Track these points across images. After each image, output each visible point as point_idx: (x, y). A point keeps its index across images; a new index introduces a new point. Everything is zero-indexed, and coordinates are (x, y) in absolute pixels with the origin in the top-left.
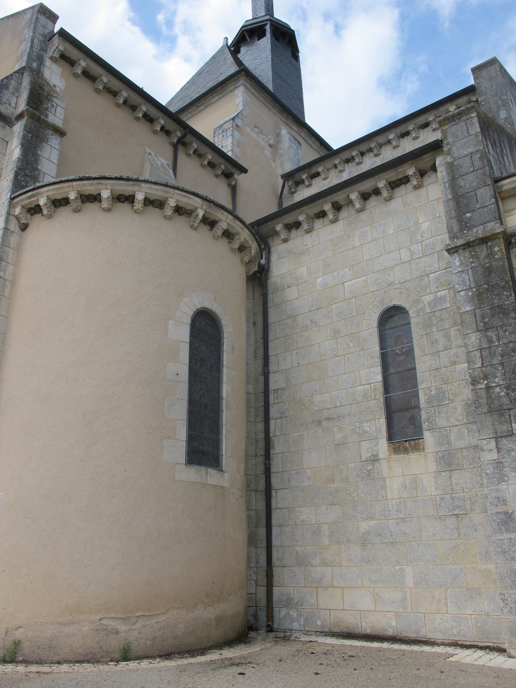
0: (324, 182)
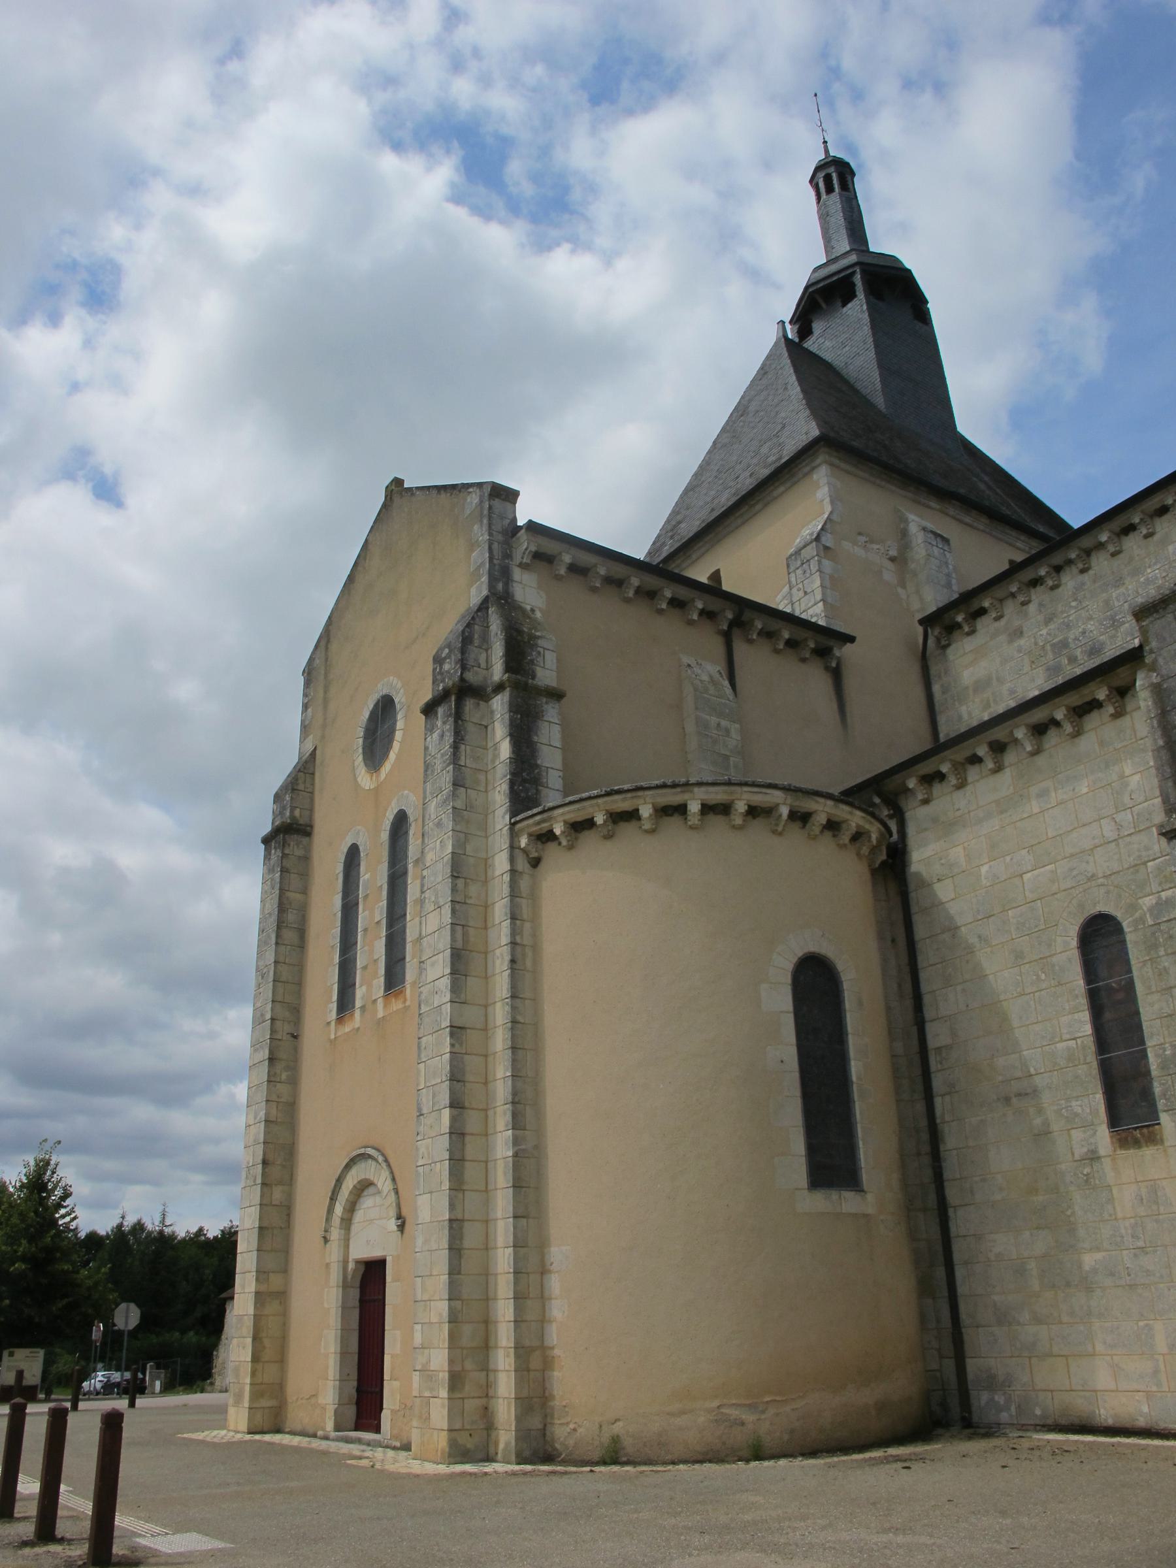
0: (997, 624)
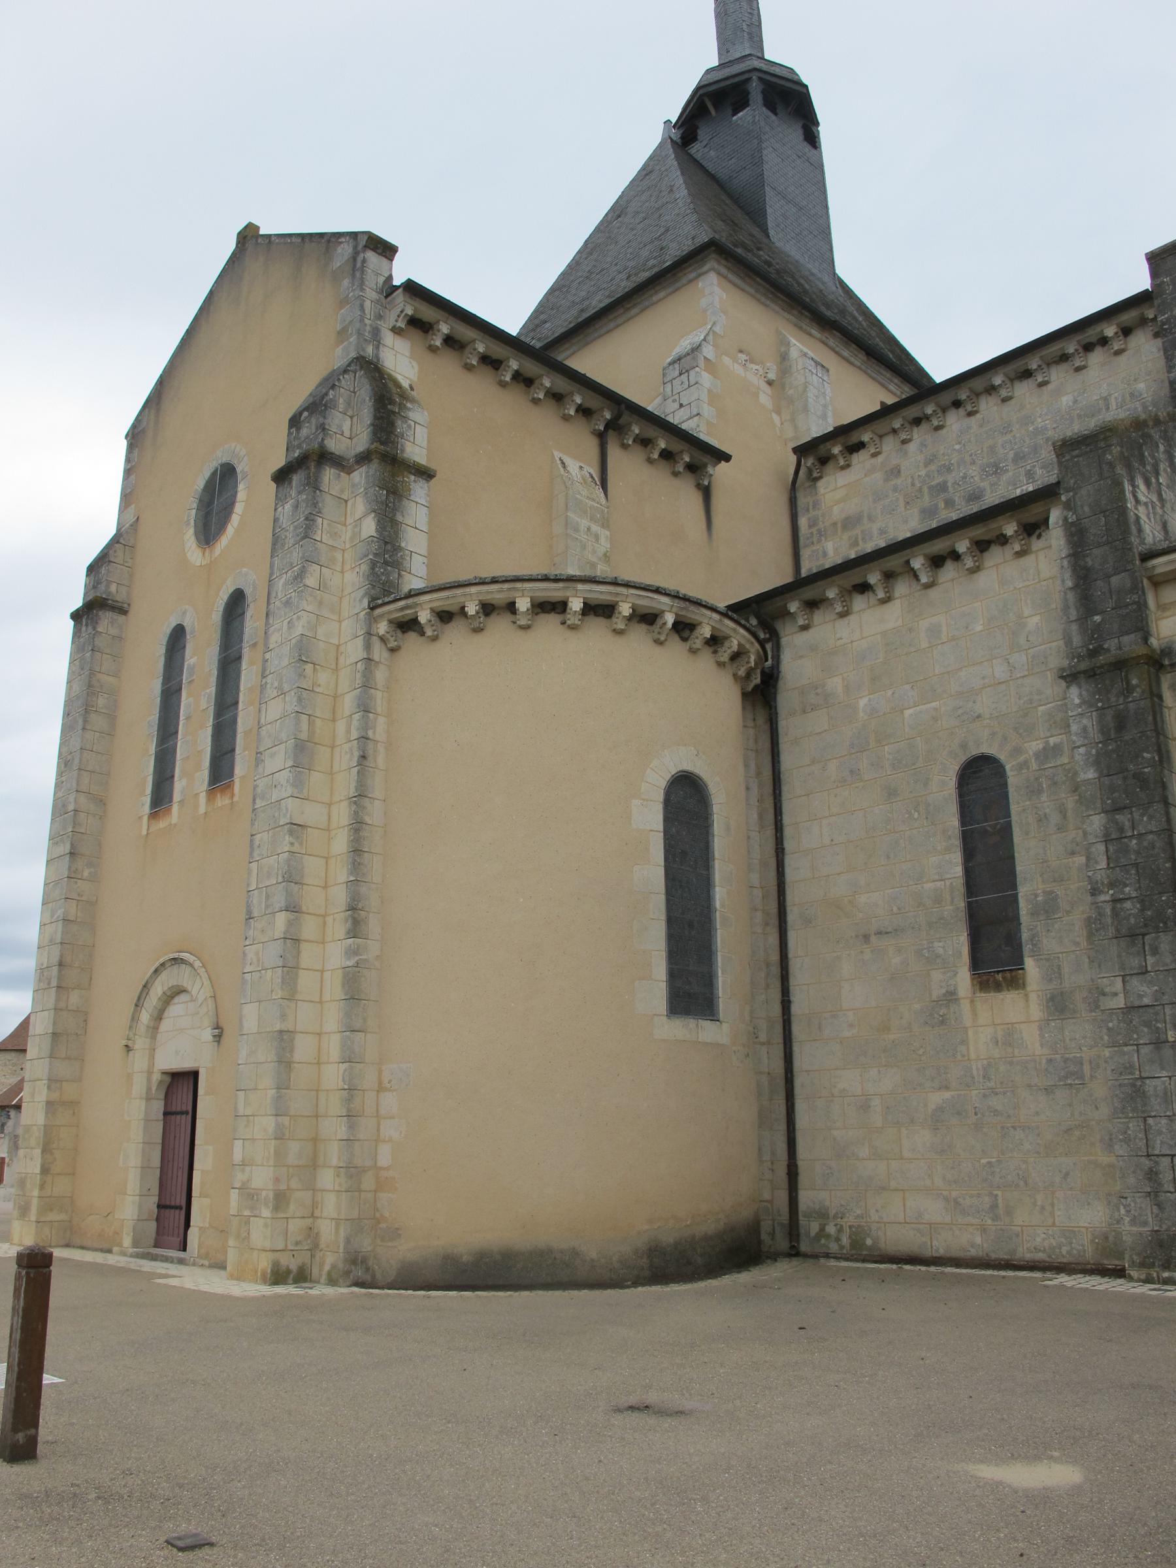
0: (873, 461)
